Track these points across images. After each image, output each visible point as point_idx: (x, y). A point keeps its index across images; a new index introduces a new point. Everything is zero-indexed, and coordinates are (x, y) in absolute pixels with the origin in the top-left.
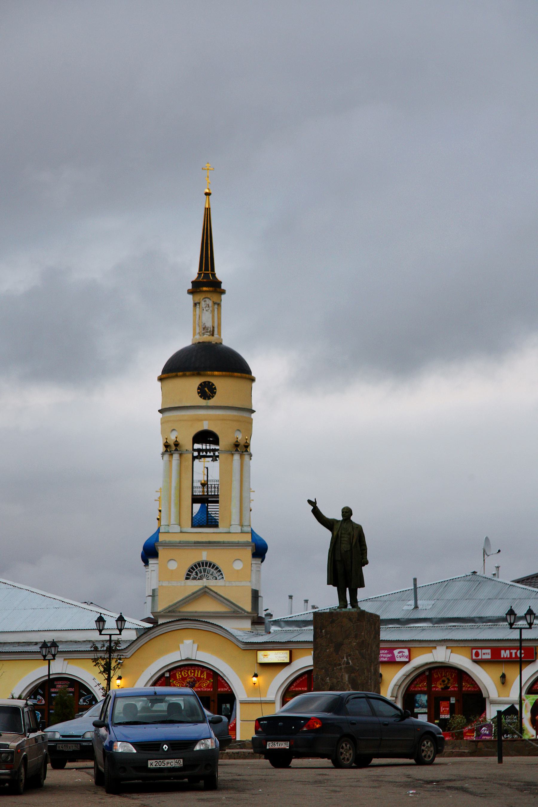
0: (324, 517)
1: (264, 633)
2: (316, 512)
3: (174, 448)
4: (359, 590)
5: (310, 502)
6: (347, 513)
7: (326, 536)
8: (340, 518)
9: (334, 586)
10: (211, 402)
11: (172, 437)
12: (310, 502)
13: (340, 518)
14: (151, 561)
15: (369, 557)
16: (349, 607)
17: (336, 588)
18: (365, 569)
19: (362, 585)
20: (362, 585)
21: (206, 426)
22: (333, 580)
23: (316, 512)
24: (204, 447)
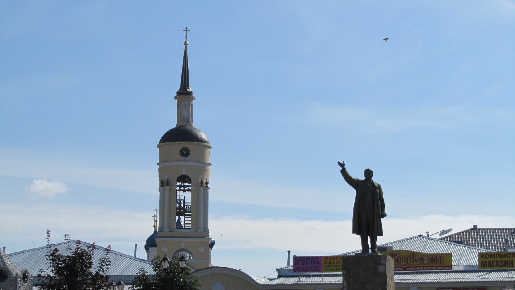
0: (351, 177)
1: (393, 246)
2: (344, 172)
3: (166, 184)
4: (378, 237)
5: (339, 164)
6: (368, 173)
7: (351, 193)
8: (362, 178)
9: (358, 234)
10: (188, 158)
11: (166, 177)
12: (339, 164)
13: (362, 178)
14: (150, 249)
15: (386, 211)
16: (370, 252)
17: (359, 236)
18: (383, 220)
19: (381, 234)
20: (381, 234)
21: (184, 173)
22: (357, 229)
23: (344, 172)
24: (183, 184)
